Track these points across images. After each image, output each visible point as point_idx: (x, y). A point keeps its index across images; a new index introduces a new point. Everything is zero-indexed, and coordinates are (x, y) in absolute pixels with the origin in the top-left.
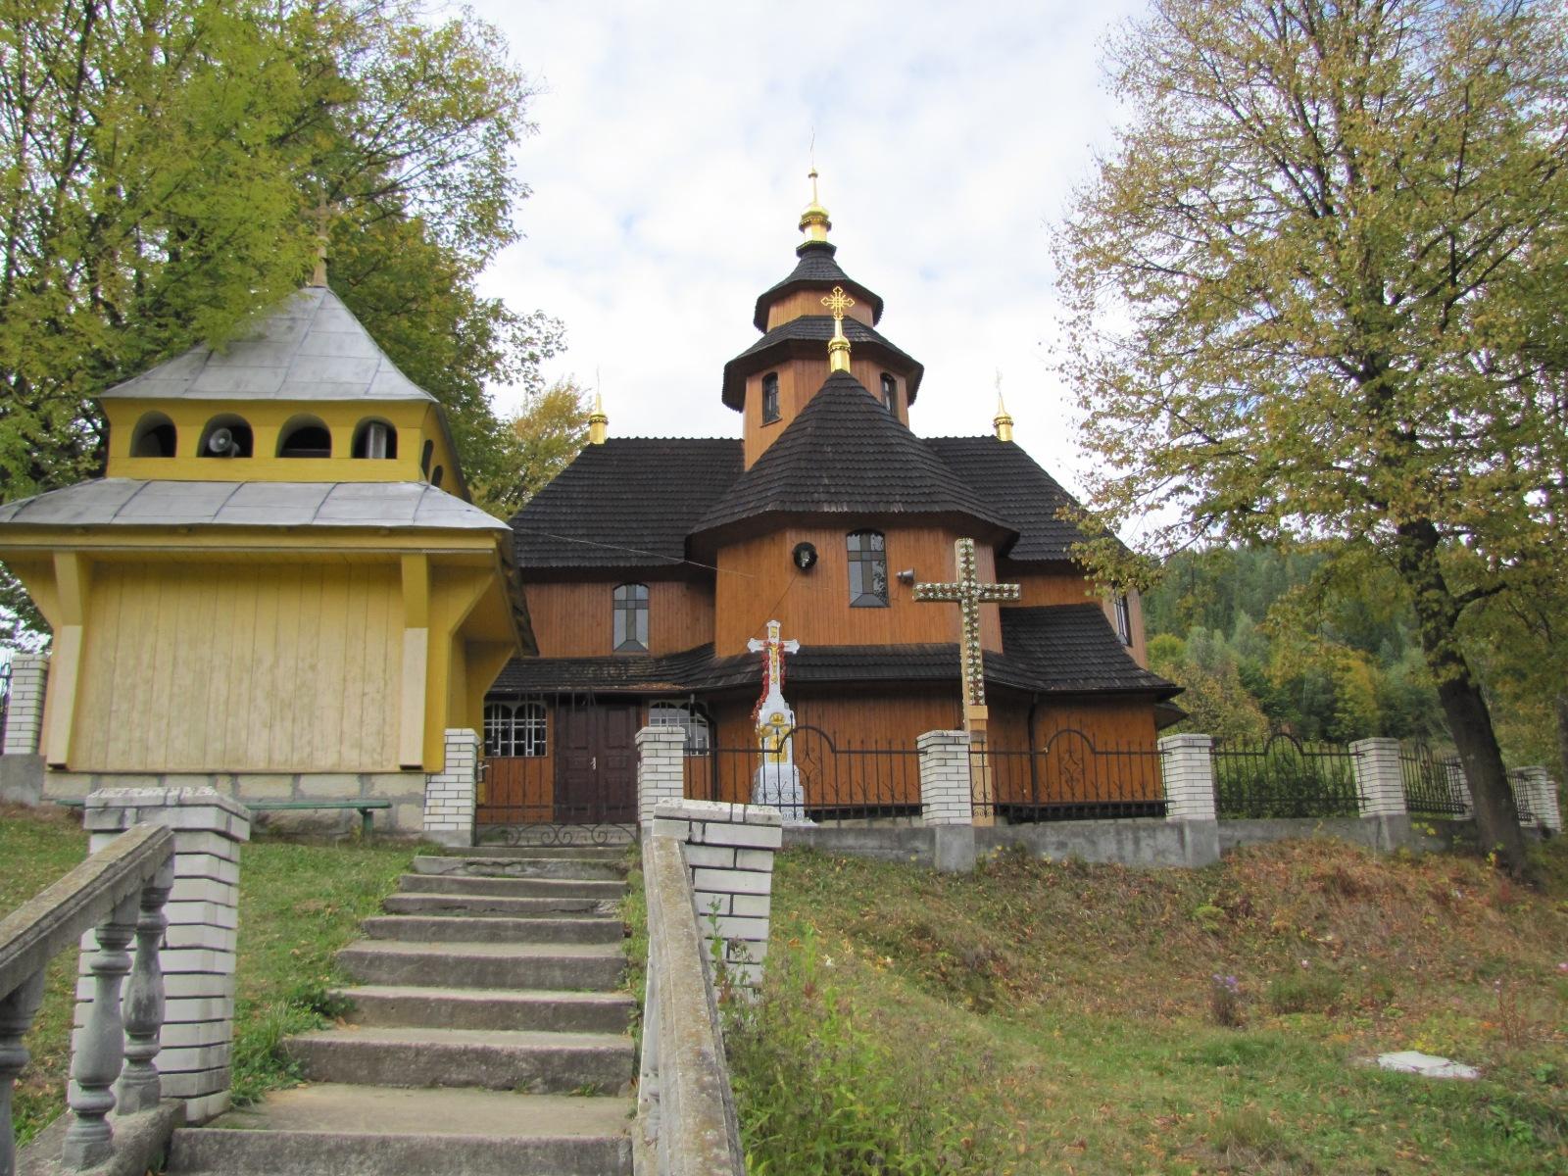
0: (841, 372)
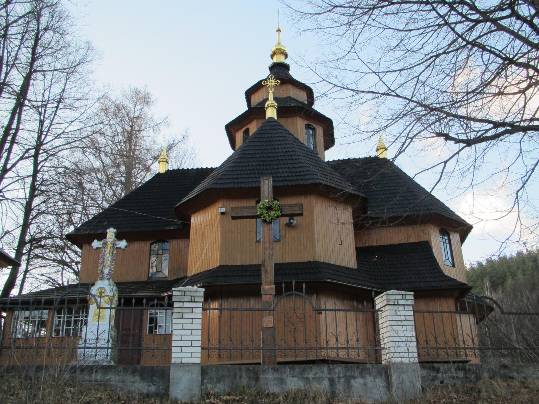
0: (271, 119)
